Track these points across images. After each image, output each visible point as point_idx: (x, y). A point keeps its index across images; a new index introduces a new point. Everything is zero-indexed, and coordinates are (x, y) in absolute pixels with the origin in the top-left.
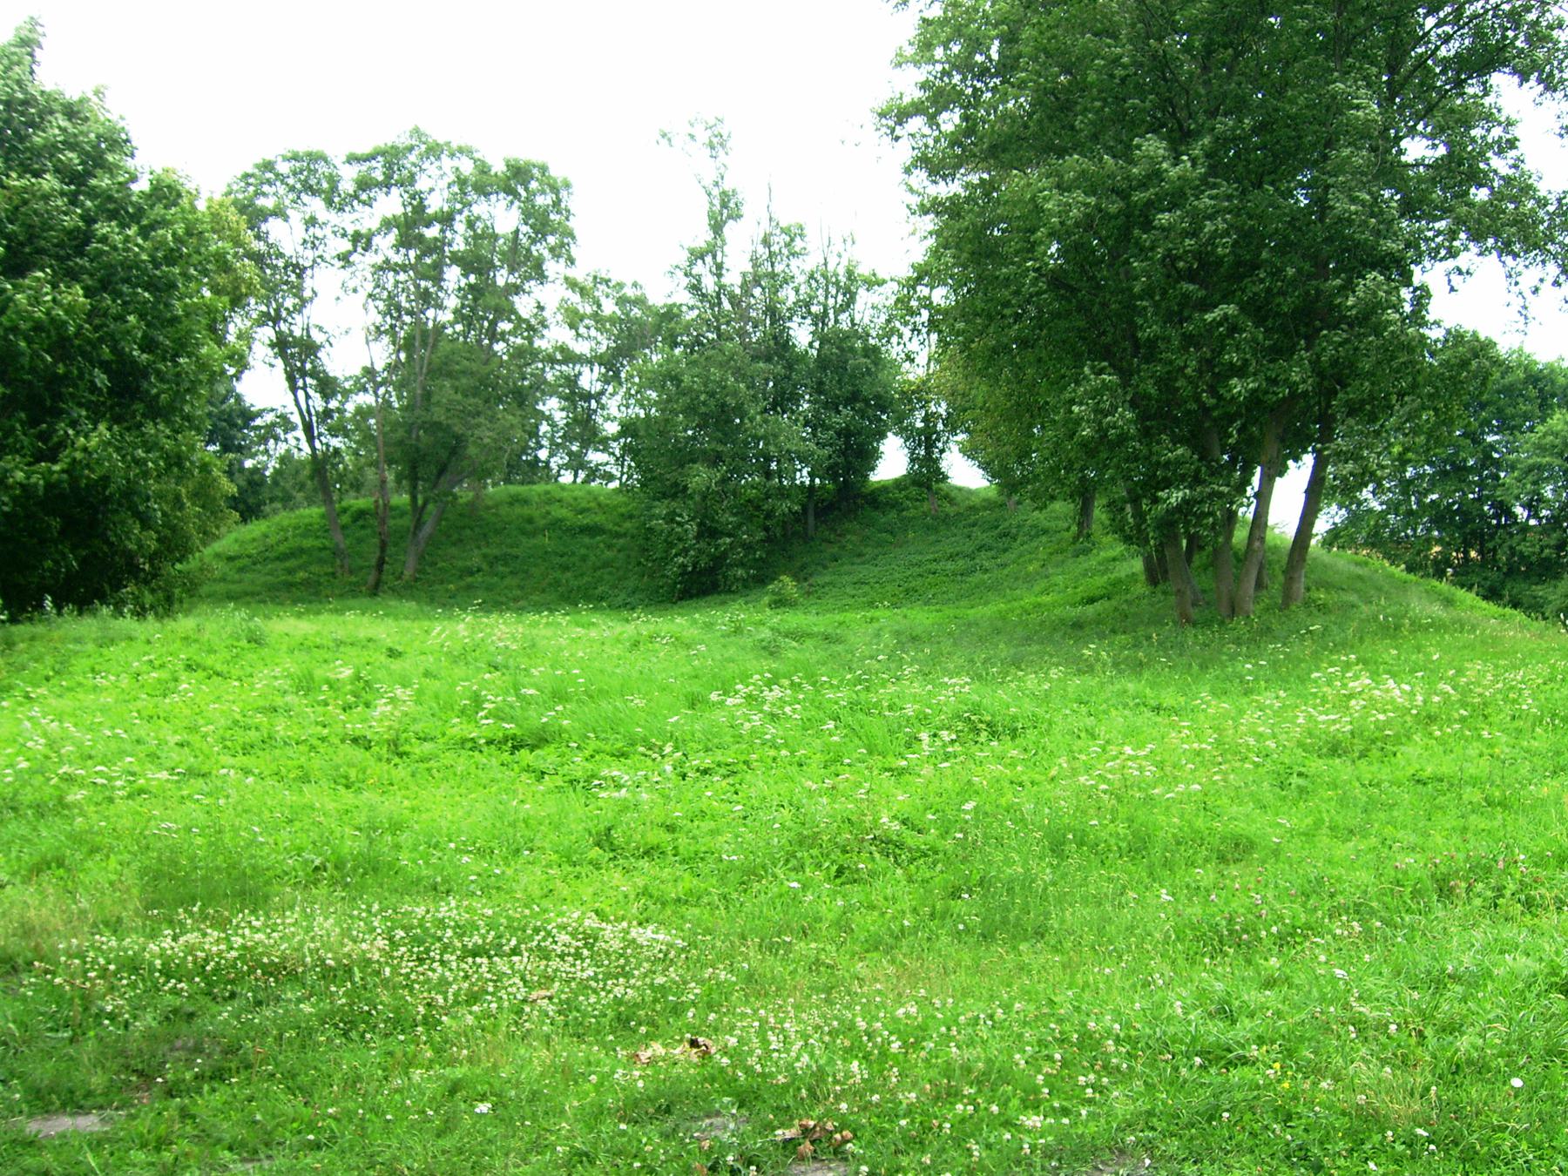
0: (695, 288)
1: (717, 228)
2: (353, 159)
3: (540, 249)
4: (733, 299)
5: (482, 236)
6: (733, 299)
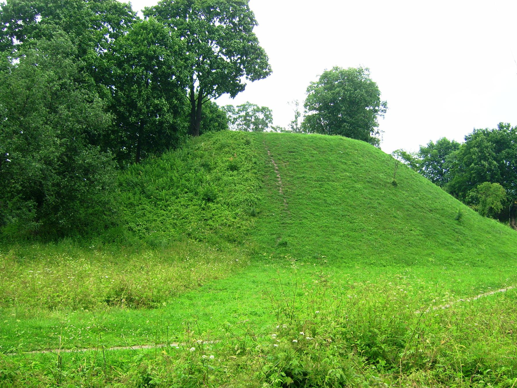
0: (293, 128)
1: (296, 118)
2: (238, 106)
3: (267, 121)
4: (299, 129)
5: (257, 119)
6: (299, 129)
